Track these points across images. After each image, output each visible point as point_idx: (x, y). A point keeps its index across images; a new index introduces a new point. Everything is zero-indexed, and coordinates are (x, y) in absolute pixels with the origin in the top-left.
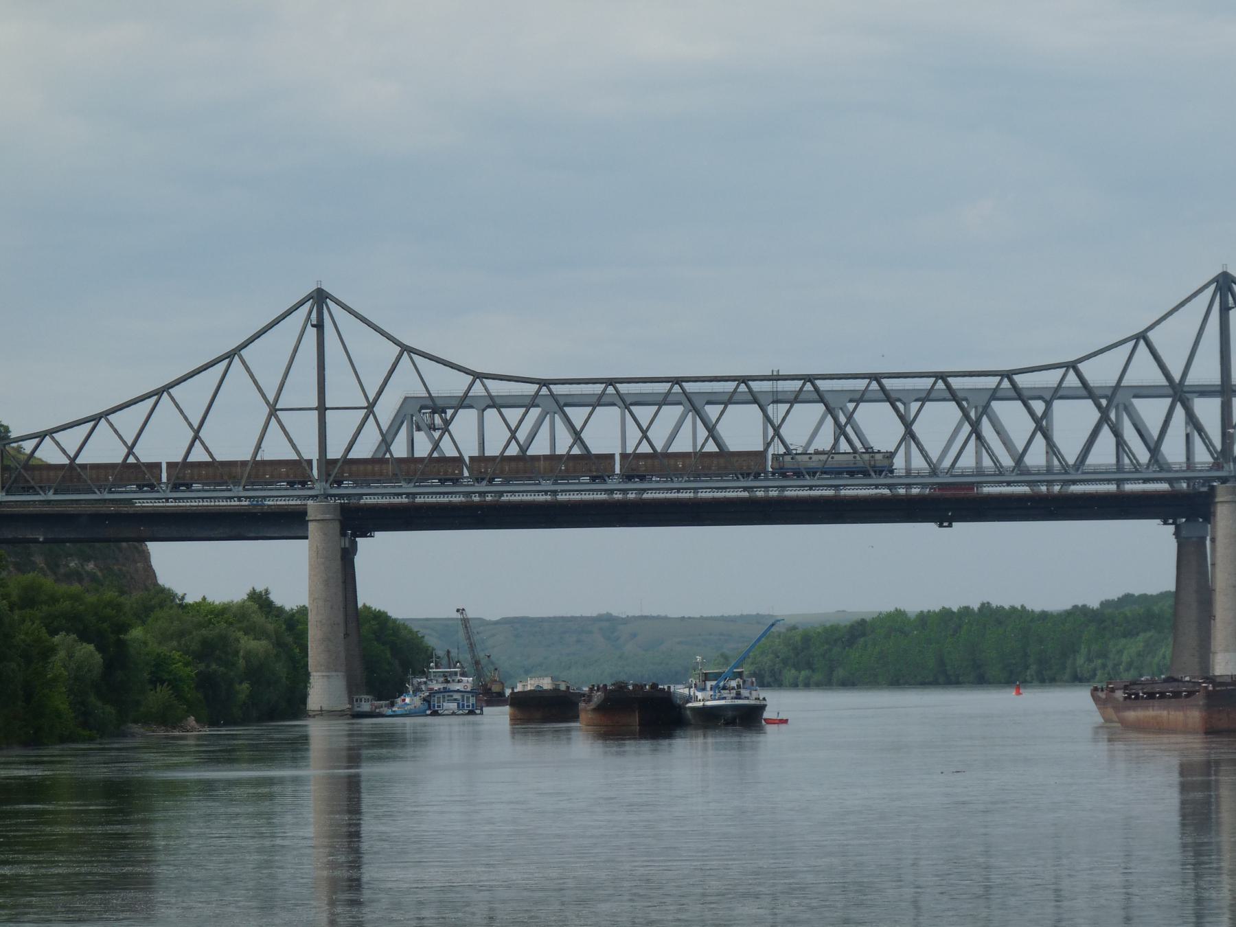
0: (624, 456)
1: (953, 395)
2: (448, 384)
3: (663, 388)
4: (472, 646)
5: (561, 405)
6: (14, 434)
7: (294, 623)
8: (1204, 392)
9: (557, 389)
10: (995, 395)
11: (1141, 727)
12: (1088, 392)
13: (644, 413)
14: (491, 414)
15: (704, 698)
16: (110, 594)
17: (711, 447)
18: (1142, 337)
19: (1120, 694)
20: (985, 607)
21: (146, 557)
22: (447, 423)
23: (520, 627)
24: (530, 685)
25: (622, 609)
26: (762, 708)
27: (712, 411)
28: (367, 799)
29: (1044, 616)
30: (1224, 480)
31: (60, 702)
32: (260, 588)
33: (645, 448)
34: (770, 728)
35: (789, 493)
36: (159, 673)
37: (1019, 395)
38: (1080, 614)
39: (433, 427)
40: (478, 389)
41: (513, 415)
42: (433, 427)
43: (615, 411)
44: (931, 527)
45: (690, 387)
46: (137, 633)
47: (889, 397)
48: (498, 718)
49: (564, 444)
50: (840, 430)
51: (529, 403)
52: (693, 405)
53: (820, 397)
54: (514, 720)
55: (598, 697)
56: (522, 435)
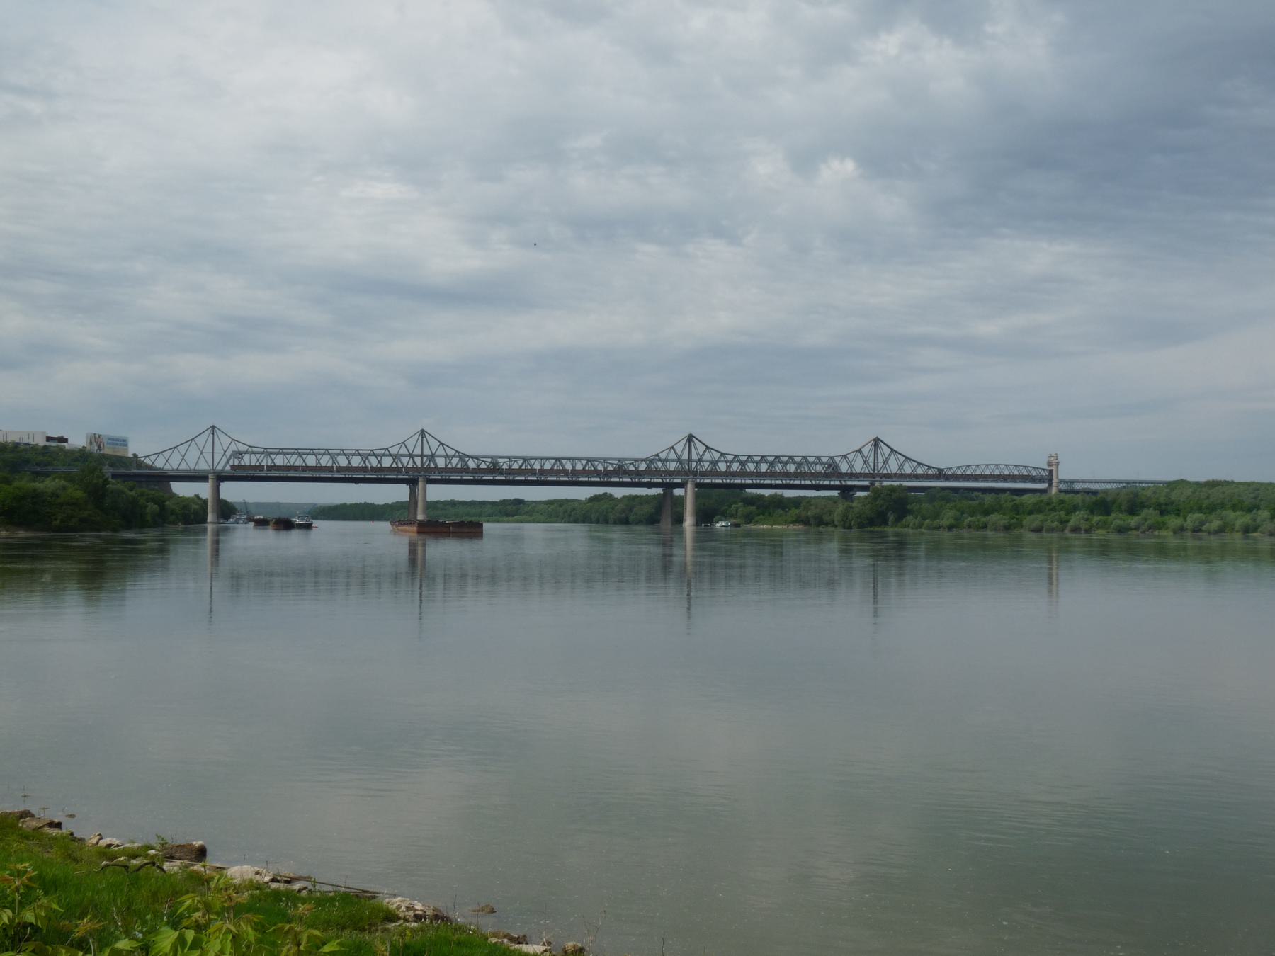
0: (267, 466)
1: (360, 455)
2: (243, 448)
3: (309, 451)
4: (247, 509)
5: (269, 454)
6: (139, 456)
7: (205, 502)
8: (417, 456)
9: (268, 450)
10: (369, 455)
11: (402, 531)
12: (390, 455)
13: (288, 456)
14: (253, 455)
15: (298, 521)
16: (161, 494)
17: (304, 465)
18: (403, 443)
19: (397, 523)
20: (365, 503)
21: (170, 486)
22: (243, 457)
23: (257, 505)
24: (258, 517)
25: (281, 501)
26: (312, 524)
27: (304, 456)
28: (221, 545)
29: (378, 505)
30: (421, 476)
31: (149, 518)
32: (197, 493)
33: (288, 464)
34: (314, 529)
35: (367, 476)
36: (173, 512)
37: (375, 455)
38: (386, 505)
39: (239, 458)
40: (250, 450)
41: (258, 456)
42: (239, 458)
43: (281, 456)
44: (354, 484)
45: (299, 451)
46: (167, 503)
47: (345, 455)
48: (252, 524)
49: (270, 463)
50: (334, 462)
51: (262, 453)
52: (300, 455)
53: (329, 454)
54: (255, 526)
55: (274, 520)
56: (260, 460)
